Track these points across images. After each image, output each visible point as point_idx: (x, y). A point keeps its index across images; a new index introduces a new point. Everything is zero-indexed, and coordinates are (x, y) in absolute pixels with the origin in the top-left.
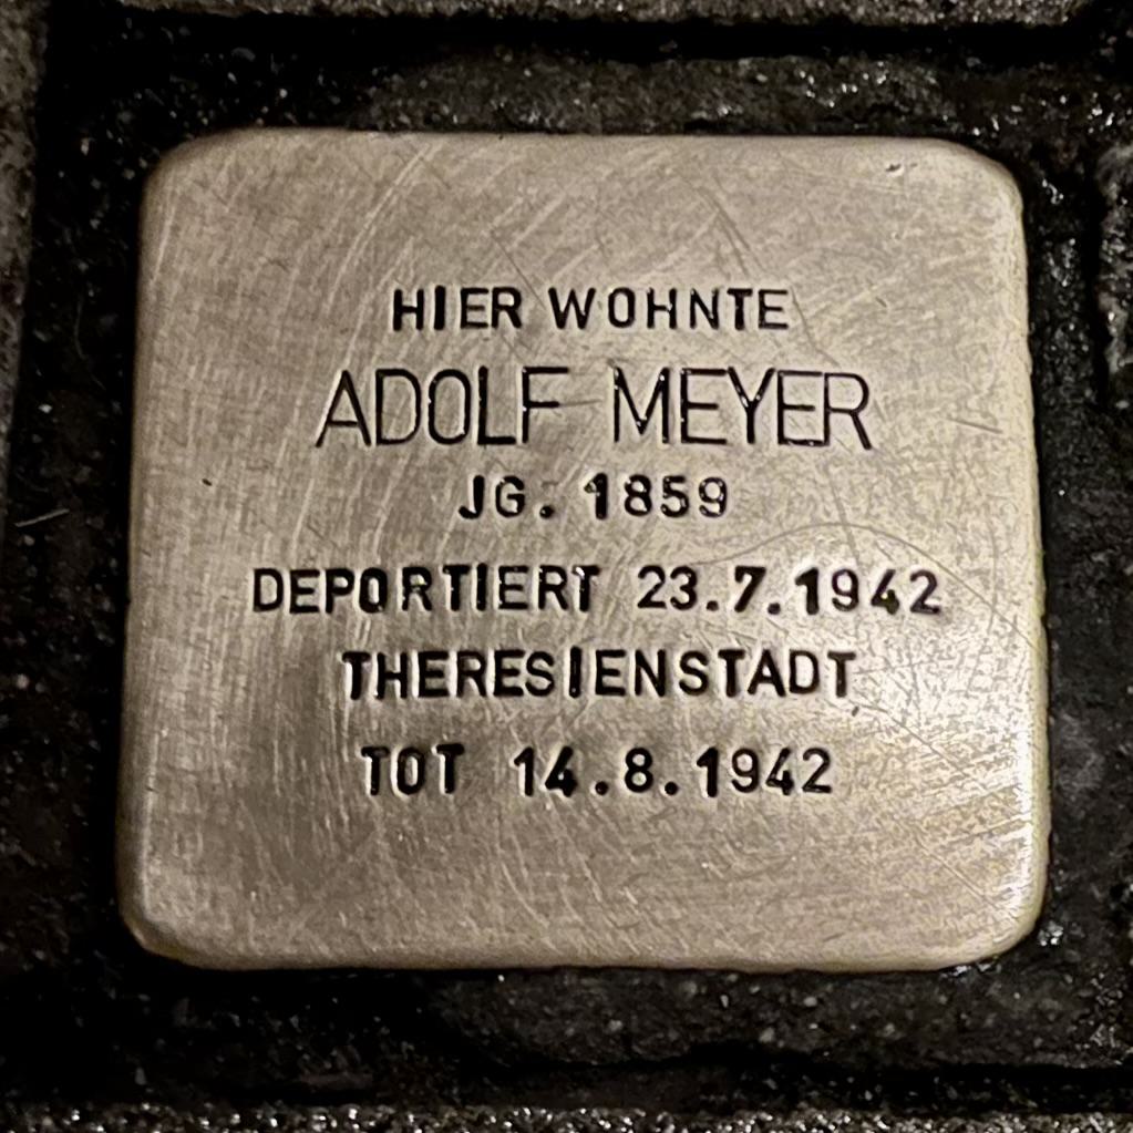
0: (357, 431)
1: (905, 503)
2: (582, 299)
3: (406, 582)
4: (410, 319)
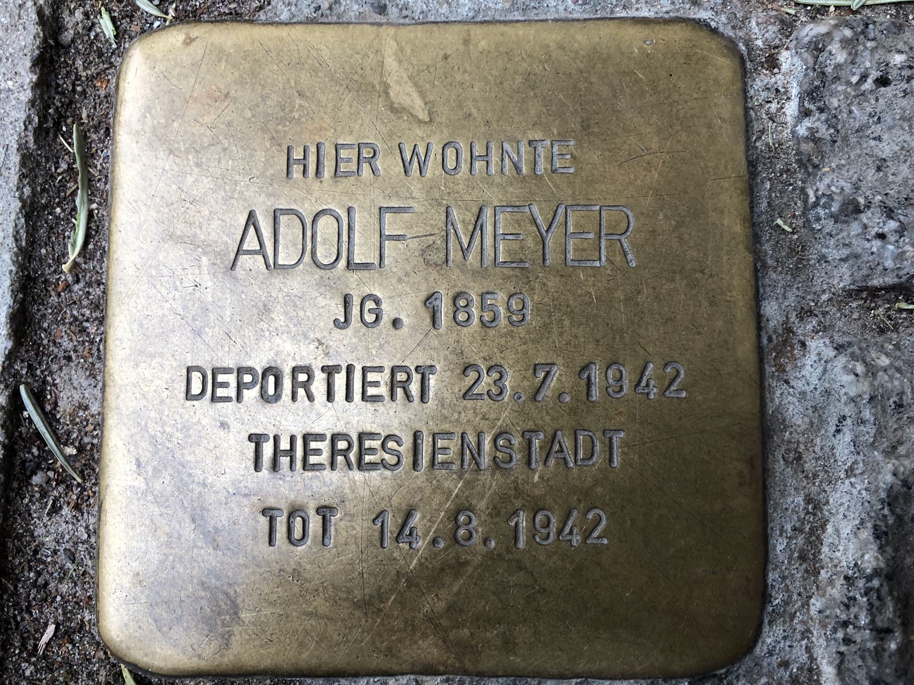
0: (260, 258)
1: (867, 157)
2: (421, 151)
3: (294, 378)
4: (297, 170)
